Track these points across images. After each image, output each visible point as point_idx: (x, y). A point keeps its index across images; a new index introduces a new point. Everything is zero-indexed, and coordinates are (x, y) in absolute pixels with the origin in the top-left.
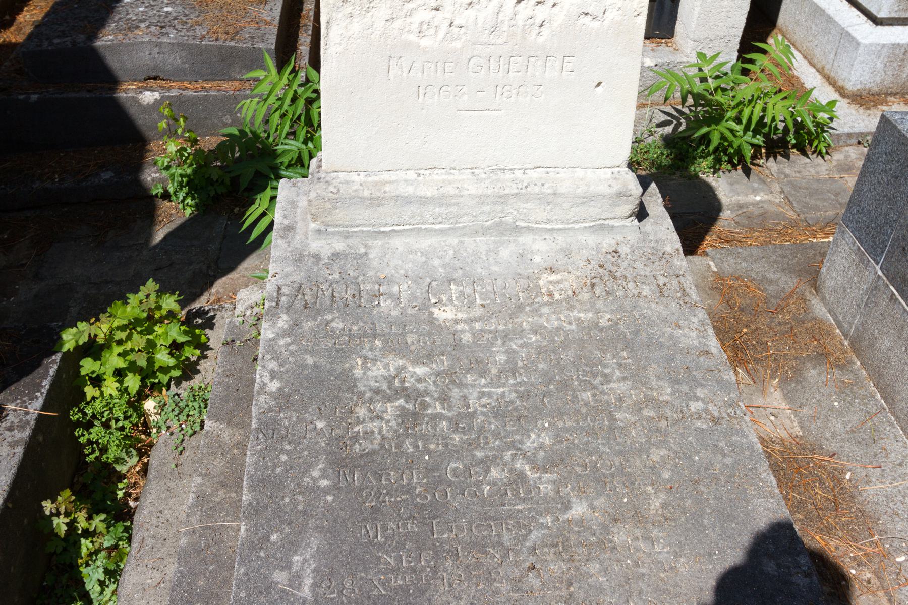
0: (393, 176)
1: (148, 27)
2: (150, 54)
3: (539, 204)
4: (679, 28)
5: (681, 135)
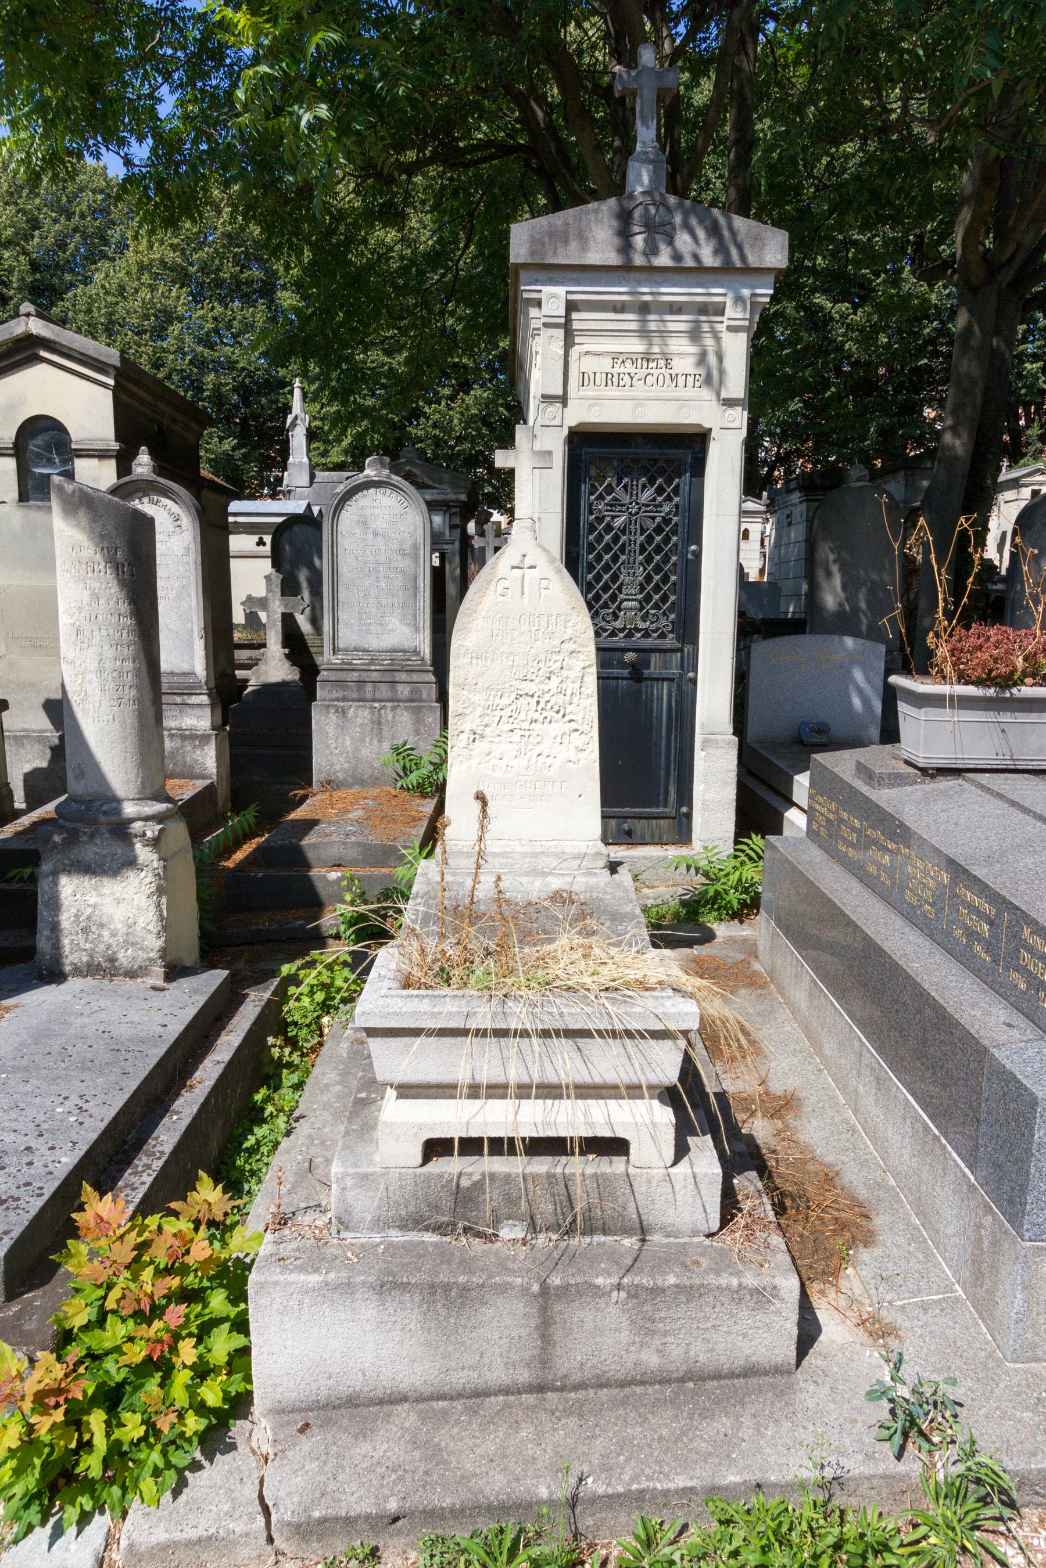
4: (694, 836)
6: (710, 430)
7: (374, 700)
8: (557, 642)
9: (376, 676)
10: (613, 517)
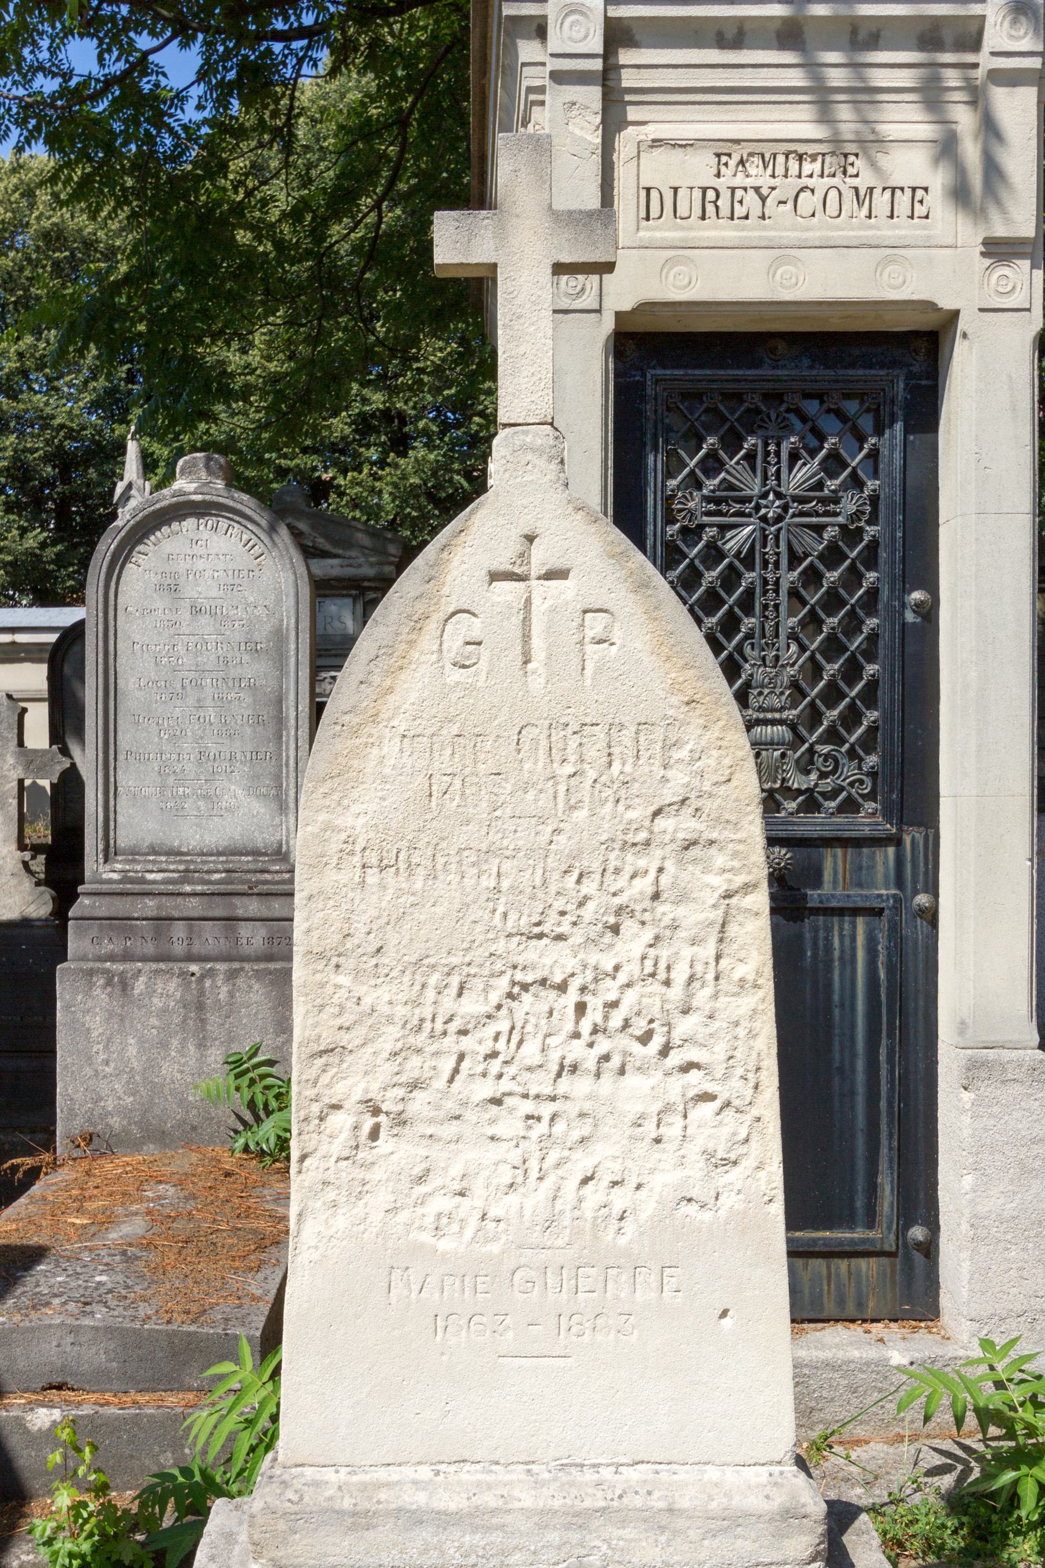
0: (394, 1474)
1: (65, 1303)
2: (58, 1346)
3: (646, 1530)
5: (973, 1489)
6: (955, 314)
7: (190, 958)
8: (639, 813)
9: (193, 906)
10: (724, 528)
